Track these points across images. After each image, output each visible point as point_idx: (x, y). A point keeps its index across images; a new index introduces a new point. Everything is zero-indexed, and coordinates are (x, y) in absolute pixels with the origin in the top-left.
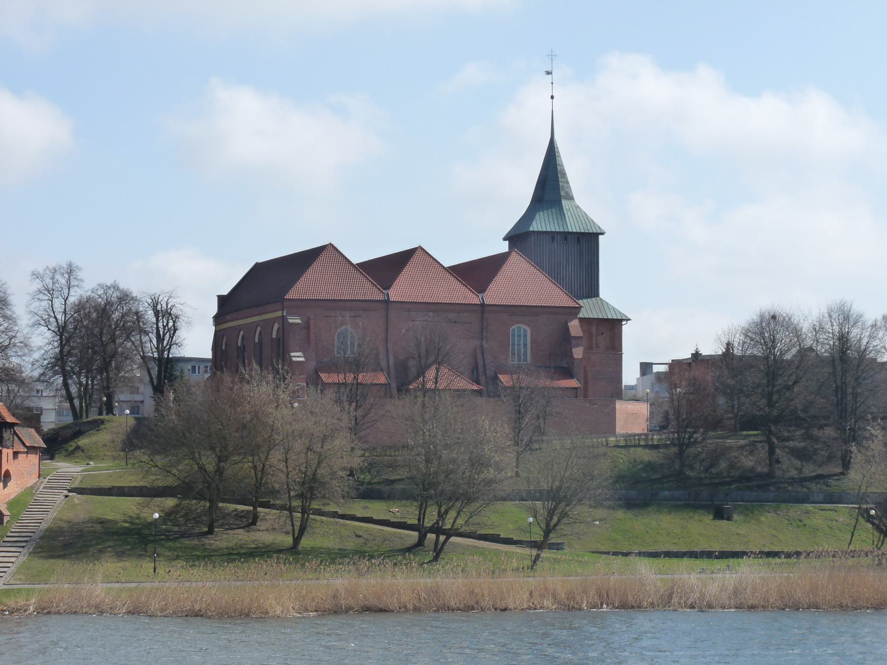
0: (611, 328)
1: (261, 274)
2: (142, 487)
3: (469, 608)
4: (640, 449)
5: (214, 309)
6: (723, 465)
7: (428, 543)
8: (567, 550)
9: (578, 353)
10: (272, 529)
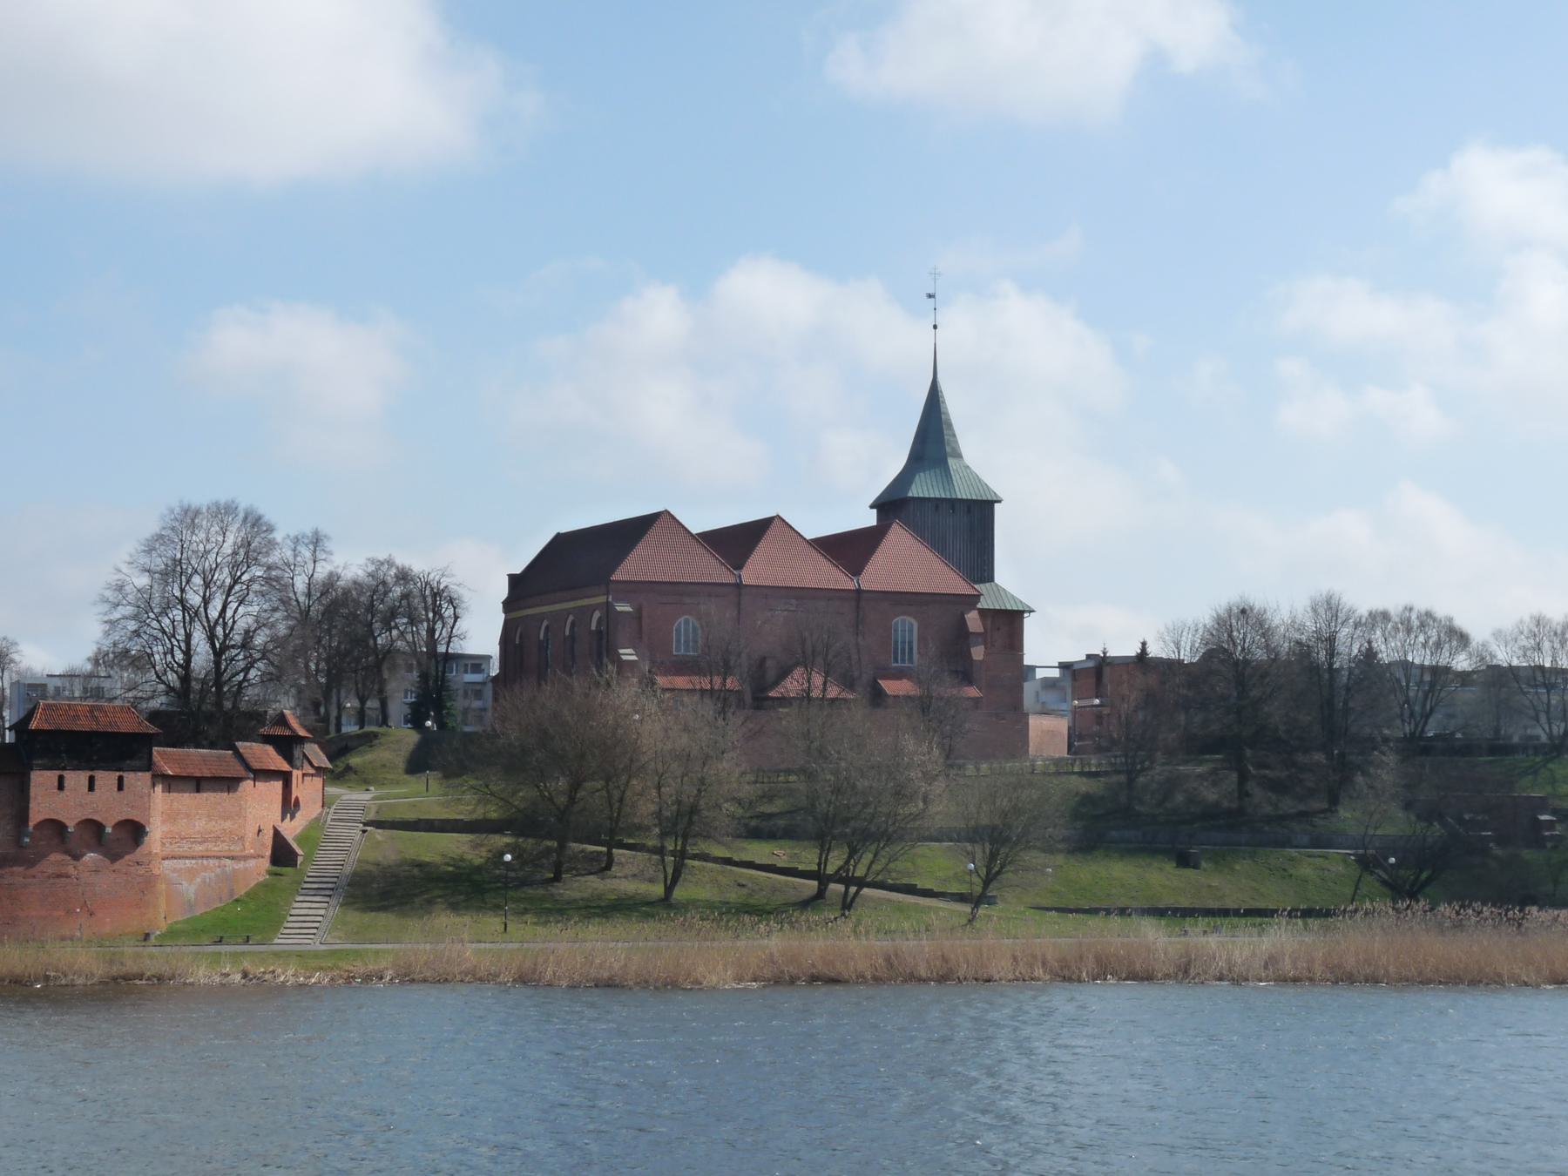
0: (1010, 622)
1: (563, 549)
2: (448, 821)
3: (942, 979)
4: (1074, 777)
5: (504, 592)
6: (1179, 798)
7: (833, 893)
8: (1000, 906)
9: (978, 653)
10: (631, 875)
